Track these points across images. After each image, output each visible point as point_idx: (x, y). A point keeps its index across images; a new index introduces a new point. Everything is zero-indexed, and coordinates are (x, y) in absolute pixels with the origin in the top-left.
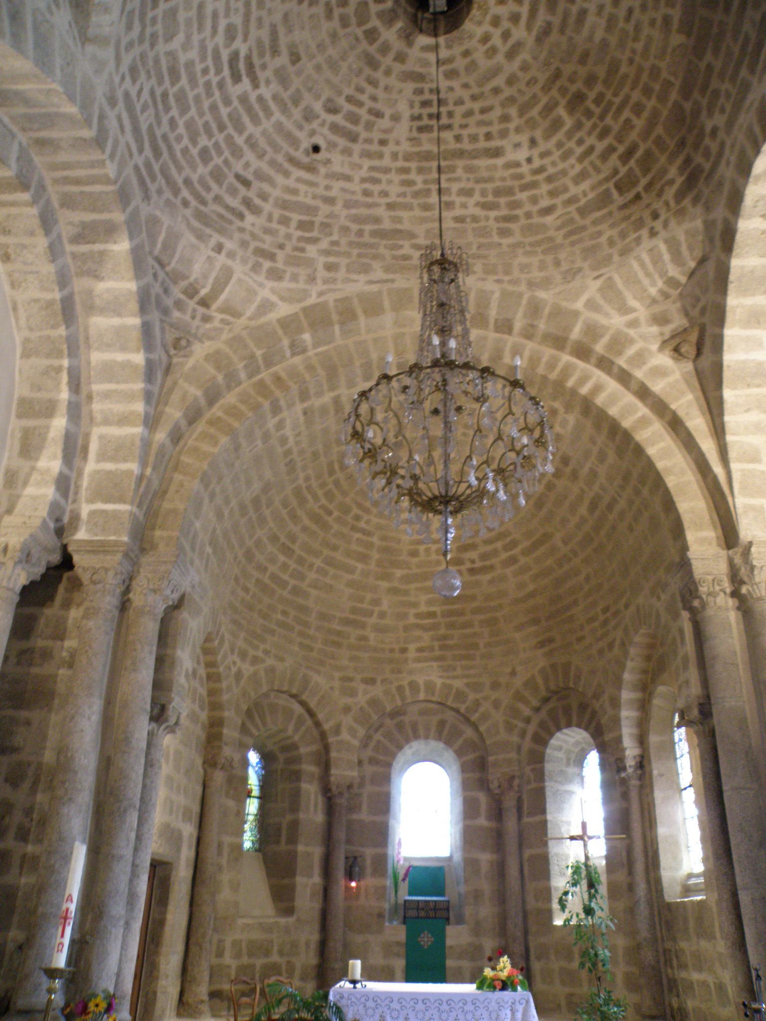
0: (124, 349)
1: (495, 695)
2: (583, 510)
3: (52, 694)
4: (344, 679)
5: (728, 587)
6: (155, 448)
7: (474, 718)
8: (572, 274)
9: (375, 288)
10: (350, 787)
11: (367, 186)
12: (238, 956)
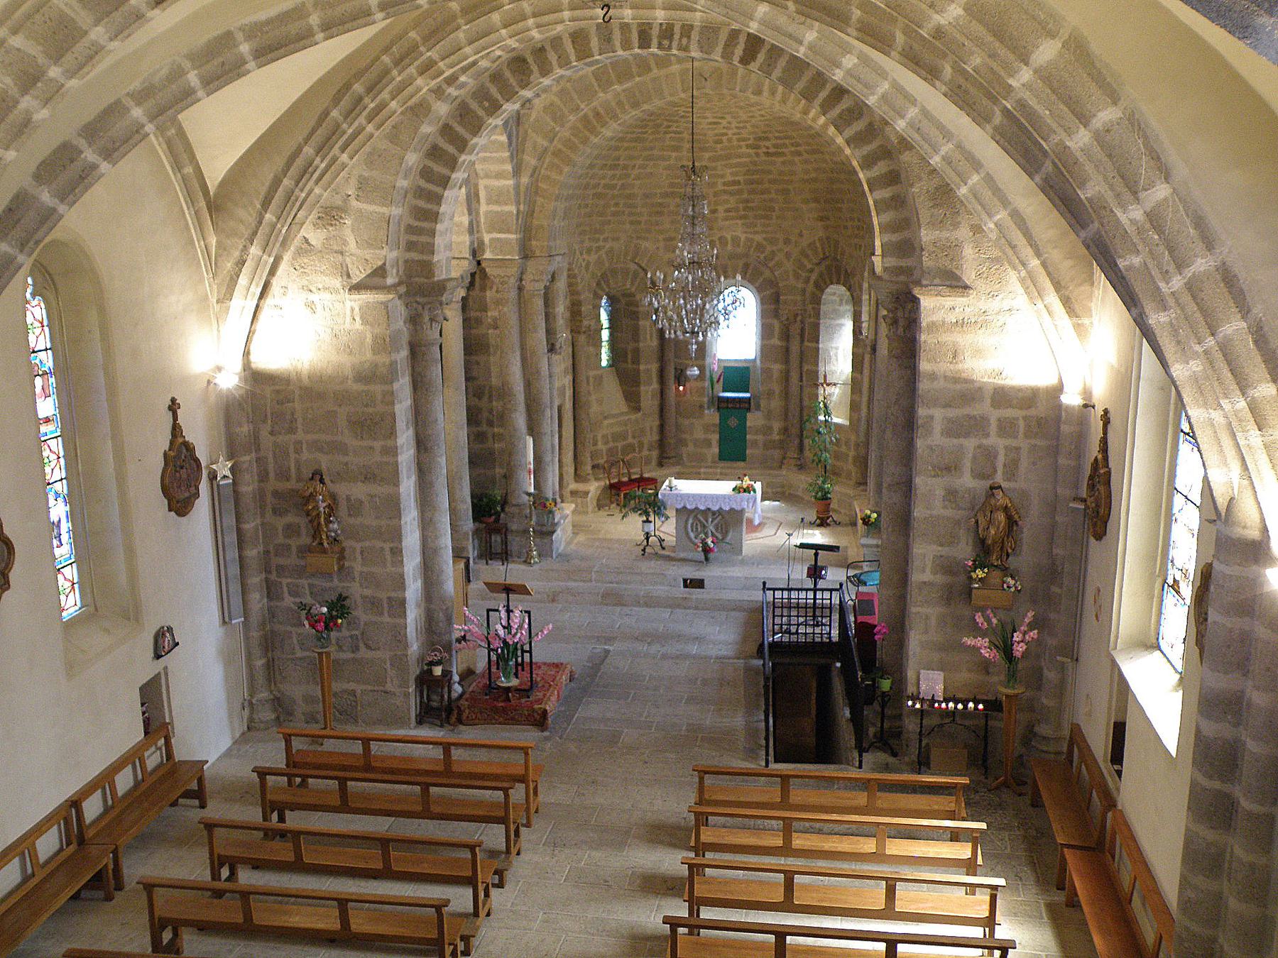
3: (488, 346)
6: (522, 189)
12: (607, 443)
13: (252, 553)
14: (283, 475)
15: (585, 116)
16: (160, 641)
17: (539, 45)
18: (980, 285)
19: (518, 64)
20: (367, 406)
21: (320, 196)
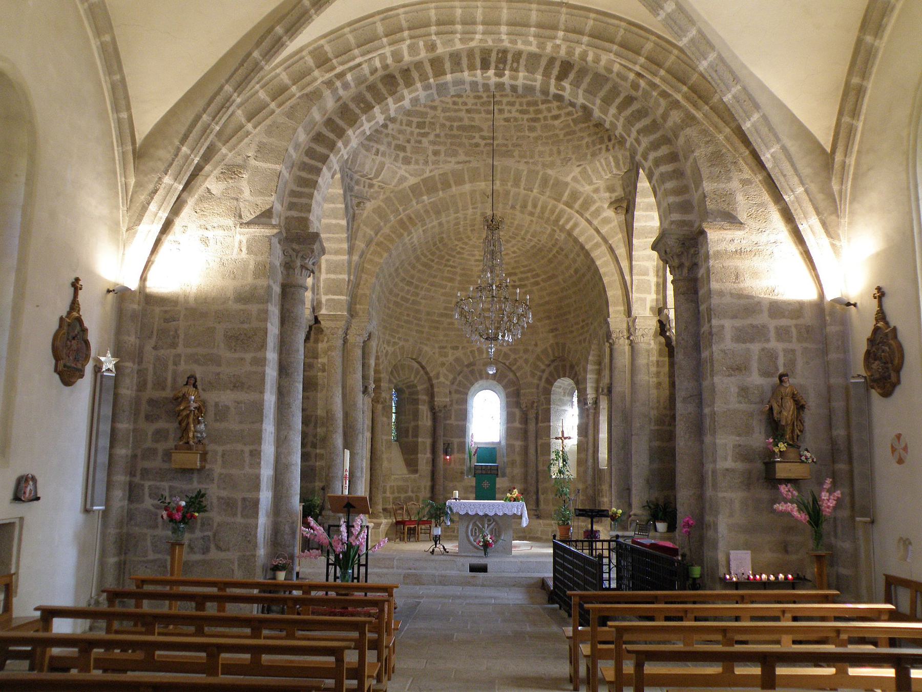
0: (336, 218)
1: (525, 356)
2: (572, 271)
4: (440, 348)
5: (626, 334)
6: (353, 264)
7: (514, 368)
8: (566, 161)
9: (460, 167)
10: (445, 406)
11: (454, 99)
12: (393, 493)
13: (122, 451)
14: (160, 384)
15: (402, 219)
16: (23, 485)
17: (406, 67)
18: (751, 222)
19: (390, 80)
20: (242, 323)
21: (226, 155)
